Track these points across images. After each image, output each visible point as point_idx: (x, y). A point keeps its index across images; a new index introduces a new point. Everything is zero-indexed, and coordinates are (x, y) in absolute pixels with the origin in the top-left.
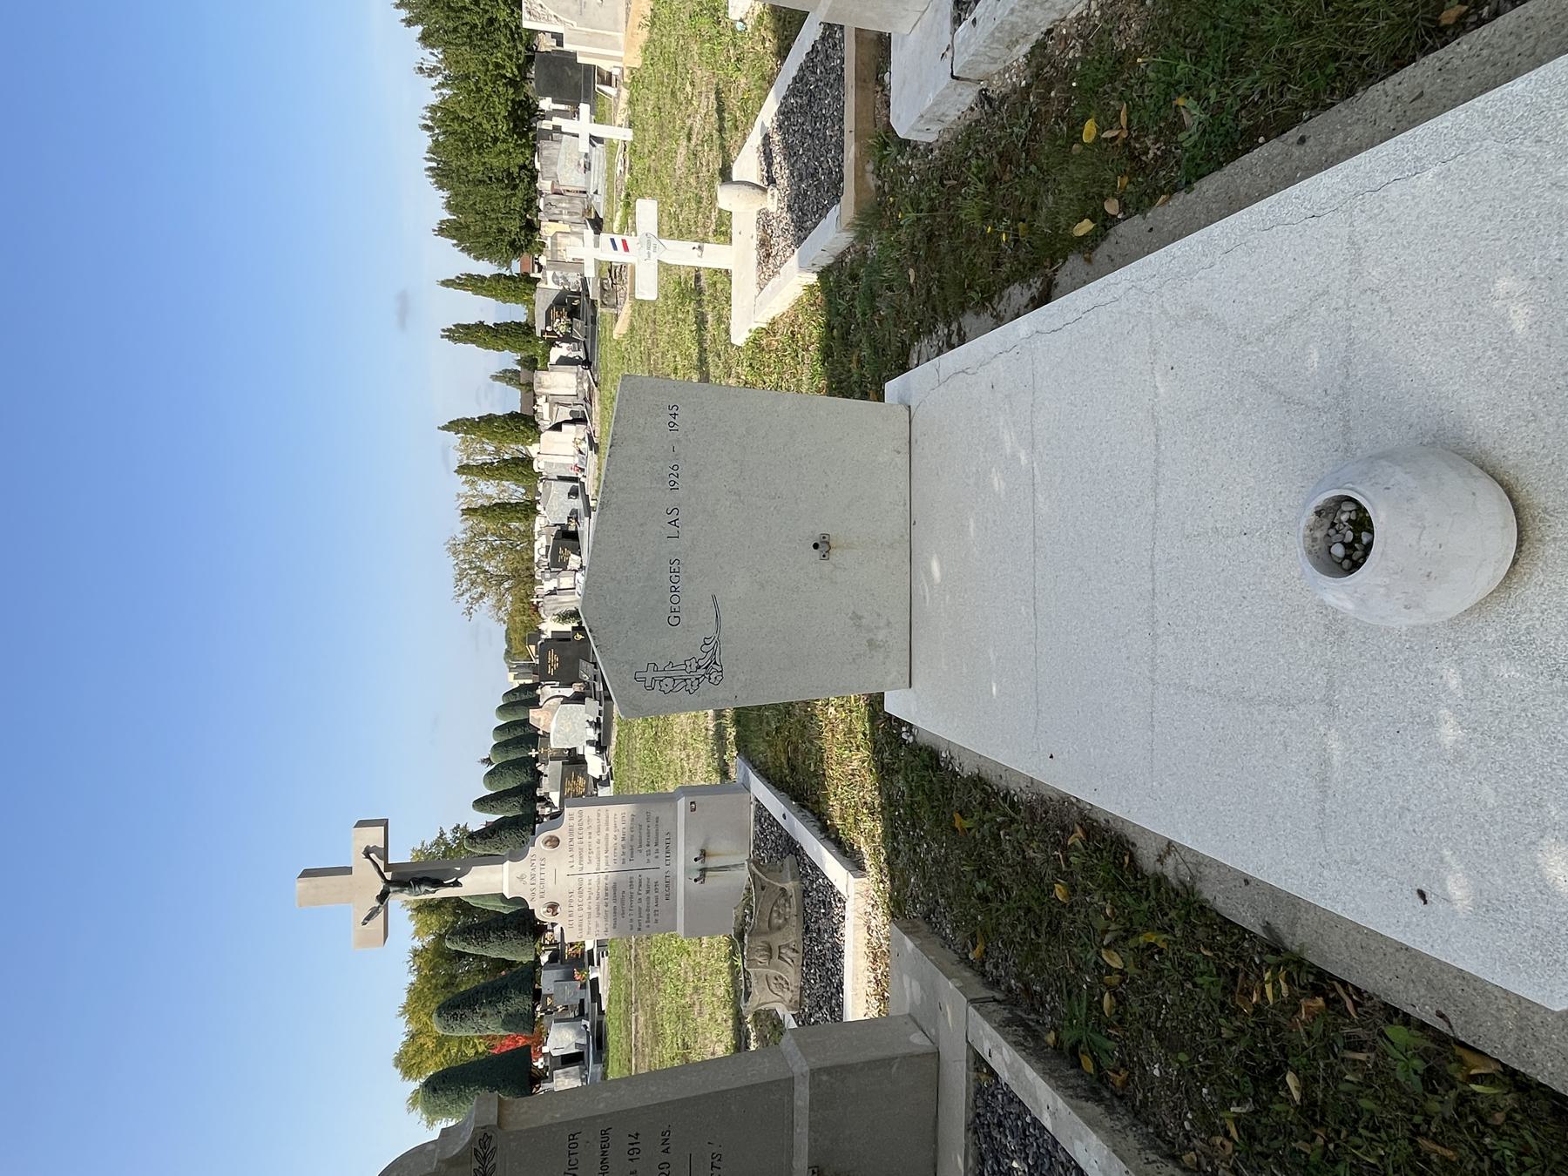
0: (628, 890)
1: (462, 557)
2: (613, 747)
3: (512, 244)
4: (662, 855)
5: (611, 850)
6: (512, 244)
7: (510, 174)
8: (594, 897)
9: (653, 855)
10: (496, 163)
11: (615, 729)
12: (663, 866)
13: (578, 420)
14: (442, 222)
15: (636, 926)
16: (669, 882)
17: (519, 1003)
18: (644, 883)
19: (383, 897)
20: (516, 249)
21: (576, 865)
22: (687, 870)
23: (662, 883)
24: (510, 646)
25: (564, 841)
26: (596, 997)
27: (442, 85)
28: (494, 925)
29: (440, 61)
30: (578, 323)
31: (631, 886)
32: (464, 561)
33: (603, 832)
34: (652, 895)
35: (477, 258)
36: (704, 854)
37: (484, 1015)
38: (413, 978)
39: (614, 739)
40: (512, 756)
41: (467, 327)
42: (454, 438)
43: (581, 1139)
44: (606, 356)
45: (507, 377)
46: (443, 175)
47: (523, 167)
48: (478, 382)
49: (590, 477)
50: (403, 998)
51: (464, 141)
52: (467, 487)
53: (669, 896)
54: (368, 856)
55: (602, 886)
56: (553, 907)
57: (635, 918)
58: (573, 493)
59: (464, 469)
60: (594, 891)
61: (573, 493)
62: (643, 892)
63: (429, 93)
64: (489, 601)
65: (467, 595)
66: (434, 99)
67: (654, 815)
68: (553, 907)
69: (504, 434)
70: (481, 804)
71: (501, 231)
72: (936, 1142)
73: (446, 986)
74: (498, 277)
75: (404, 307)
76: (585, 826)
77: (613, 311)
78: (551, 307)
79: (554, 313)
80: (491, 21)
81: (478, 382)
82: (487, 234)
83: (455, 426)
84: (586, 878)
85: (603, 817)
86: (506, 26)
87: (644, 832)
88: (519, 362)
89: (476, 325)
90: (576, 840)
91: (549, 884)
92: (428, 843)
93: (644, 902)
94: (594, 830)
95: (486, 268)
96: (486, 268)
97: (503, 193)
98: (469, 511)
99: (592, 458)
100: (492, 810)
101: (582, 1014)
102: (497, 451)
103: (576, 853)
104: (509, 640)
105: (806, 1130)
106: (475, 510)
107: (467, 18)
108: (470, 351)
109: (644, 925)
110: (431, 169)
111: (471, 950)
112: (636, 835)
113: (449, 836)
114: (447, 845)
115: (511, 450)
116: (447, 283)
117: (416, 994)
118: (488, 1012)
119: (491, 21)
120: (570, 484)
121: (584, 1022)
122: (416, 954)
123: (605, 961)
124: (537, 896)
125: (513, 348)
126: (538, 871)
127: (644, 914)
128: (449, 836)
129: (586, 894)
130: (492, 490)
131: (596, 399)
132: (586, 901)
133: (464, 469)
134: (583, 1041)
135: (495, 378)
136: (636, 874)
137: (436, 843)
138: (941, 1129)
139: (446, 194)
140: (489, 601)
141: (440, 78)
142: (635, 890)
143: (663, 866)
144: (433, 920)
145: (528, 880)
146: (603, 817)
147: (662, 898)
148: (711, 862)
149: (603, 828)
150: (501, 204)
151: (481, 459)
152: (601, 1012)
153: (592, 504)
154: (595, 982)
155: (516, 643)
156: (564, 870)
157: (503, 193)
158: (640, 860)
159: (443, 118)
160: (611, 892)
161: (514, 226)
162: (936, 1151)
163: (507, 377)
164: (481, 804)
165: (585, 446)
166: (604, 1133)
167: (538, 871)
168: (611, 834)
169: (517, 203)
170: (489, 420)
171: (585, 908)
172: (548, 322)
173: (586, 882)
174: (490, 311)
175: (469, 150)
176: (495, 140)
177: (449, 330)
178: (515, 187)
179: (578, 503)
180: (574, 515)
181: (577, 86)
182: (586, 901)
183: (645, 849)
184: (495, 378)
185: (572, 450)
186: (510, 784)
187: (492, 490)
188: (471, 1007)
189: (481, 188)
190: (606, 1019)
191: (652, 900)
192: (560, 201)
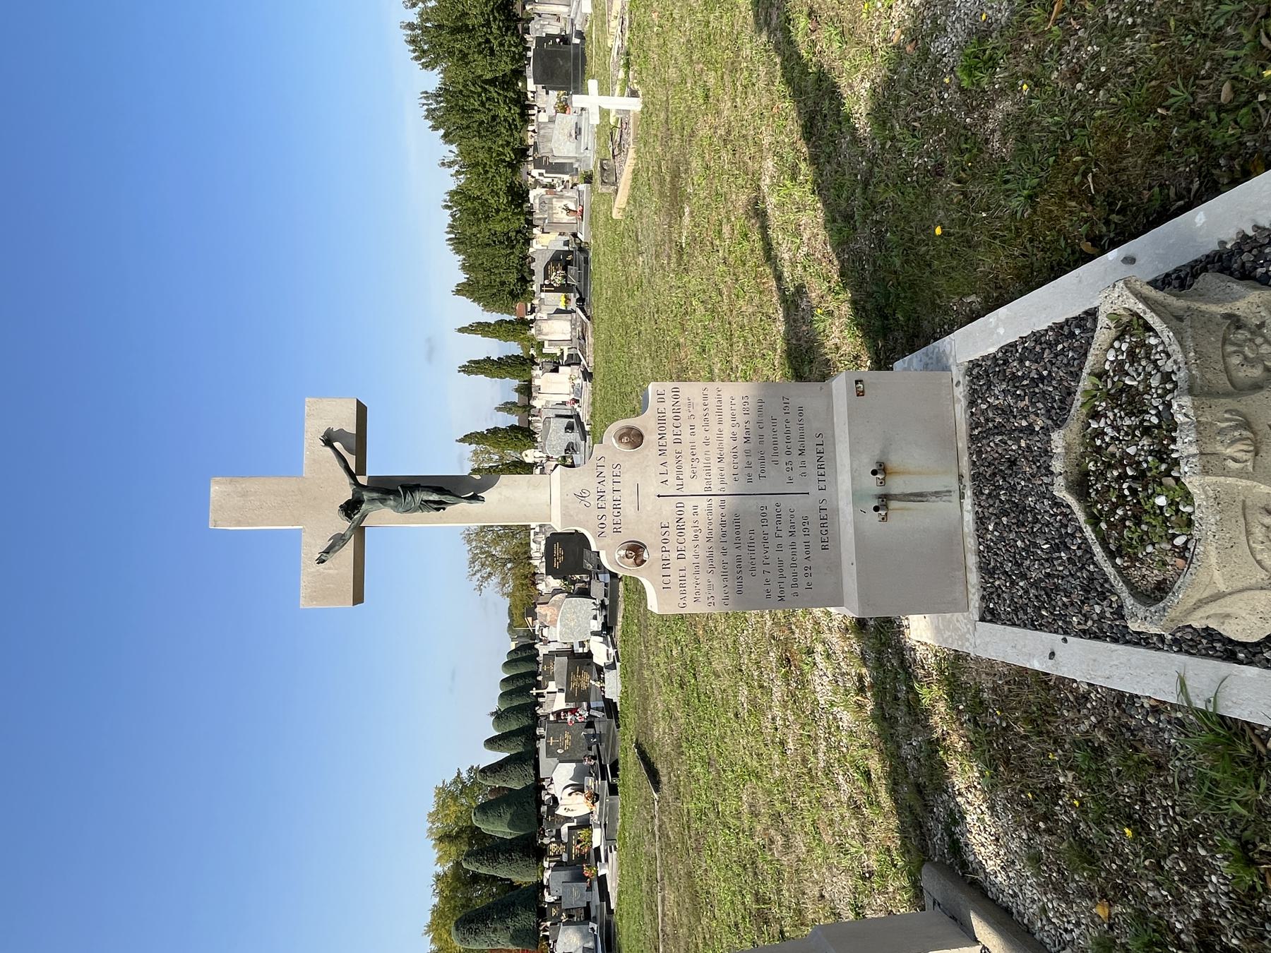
0: (759, 529)
1: (474, 544)
2: (619, 627)
3: (511, 293)
4: (812, 470)
5: (728, 459)
6: (511, 293)
7: (509, 238)
8: (702, 537)
9: (795, 474)
11: (621, 606)
12: (813, 490)
13: (573, 361)
15: (775, 593)
16: (826, 517)
17: (525, 919)
18: (785, 517)
19: (350, 508)
20: (514, 296)
21: (672, 478)
22: (857, 496)
23: (814, 519)
24: (512, 620)
25: (651, 437)
26: (604, 895)
27: (481, 328)
28: (503, 848)
29: (457, 156)
30: (572, 270)
31: (764, 521)
32: (476, 547)
33: (714, 428)
34: (800, 540)
36: (881, 469)
37: (495, 930)
38: (436, 900)
39: (620, 619)
40: (515, 703)
44: (598, 307)
45: (508, 407)
46: (459, 243)
47: (518, 232)
49: (585, 405)
50: (428, 918)
53: (828, 541)
55: (716, 518)
56: (636, 550)
57: (774, 576)
58: (570, 428)
60: (703, 525)
61: (570, 428)
62: (785, 534)
63: (449, 181)
64: (495, 580)
65: (478, 575)
66: (452, 185)
67: (795, 402)
68: (636, 550)
69: (506, 443)
70: (491, 743)
71: (503, 283)
73: (463, 906)
74: (500, 323)
76: (684, 414)
78: (548, 264)
79: (551, 267)
80: (494, 118)
83: (468, 438)
84: (689, 503)
85: (712, 401)
86: (505, 120)
87: (781, 427)
88: (516, 390)
89: (484, 360)
90: (670, 438)
91: (628, 509)
92: (448, 781)
93: (787, 551)
94: (698, 423)
96: (492, 317)
97: (503, 252)
99: (587, 386)
100: (499, 748)
101: (588, 917)
102: (501, 458)
103: (671, 461)
104: (511, 615)
107: (477, 117)
108: (481, 381)
109: (788, 591)
110: (450, 239)
111: (483, 870)
112: (767, 433)
113: (465, 775)
114: (463, 783)
115: (511, 455)
116: (462, 330)
117: (438, 913)
118: (499, 926)
119: (494, 118)
120: (567, 420)
121: (591, 924)
122: (439, 878)
123: (613, 856)
124: (609, 530)
125: (513, 376)
126: (608, 486)
127: (788, 573)
128: (465, 775)
129: (689, 533)
132: (689, 544)
134: (591, 945)
135: (499, 409)
136: (770, 502)
137: (455, 782)
139: (462, 257)
140: (495, 580)
141: (457, 167)
142: (771, 529)
143: (813, 490)
145: (592, 499)
146: (712, 401)
147: (816, 545)
148: (897, 485)
149: (713, 418)
152: (610, 911)
153: (587, 428)
154: (602, 880)
155: (517, 619)
156: (652, 487)
157: (503, 252)
158: (775, 480)
159: (459, 197)
160: (730, 530)
161: (513, 277)
163: (508, 407)
164: (491, 743)
167: (608, 486)
168: (727, 430)
169: (514, 260)
170: (495, 431)
171: (689, 554)
172: (546, 276)
173: (688, 510)
174: (494, 348)
175: (479, 220)
176: (498, 211)
178: (513, 247)
179: (575, 436)
181: (567, 74)
182: (689, 544)
183: (783, 459)
184: (499, 409)
185: (567, 388)
186: (514, 726)
188: (484, 922)
190: (616, 918)
191: (800, 548)
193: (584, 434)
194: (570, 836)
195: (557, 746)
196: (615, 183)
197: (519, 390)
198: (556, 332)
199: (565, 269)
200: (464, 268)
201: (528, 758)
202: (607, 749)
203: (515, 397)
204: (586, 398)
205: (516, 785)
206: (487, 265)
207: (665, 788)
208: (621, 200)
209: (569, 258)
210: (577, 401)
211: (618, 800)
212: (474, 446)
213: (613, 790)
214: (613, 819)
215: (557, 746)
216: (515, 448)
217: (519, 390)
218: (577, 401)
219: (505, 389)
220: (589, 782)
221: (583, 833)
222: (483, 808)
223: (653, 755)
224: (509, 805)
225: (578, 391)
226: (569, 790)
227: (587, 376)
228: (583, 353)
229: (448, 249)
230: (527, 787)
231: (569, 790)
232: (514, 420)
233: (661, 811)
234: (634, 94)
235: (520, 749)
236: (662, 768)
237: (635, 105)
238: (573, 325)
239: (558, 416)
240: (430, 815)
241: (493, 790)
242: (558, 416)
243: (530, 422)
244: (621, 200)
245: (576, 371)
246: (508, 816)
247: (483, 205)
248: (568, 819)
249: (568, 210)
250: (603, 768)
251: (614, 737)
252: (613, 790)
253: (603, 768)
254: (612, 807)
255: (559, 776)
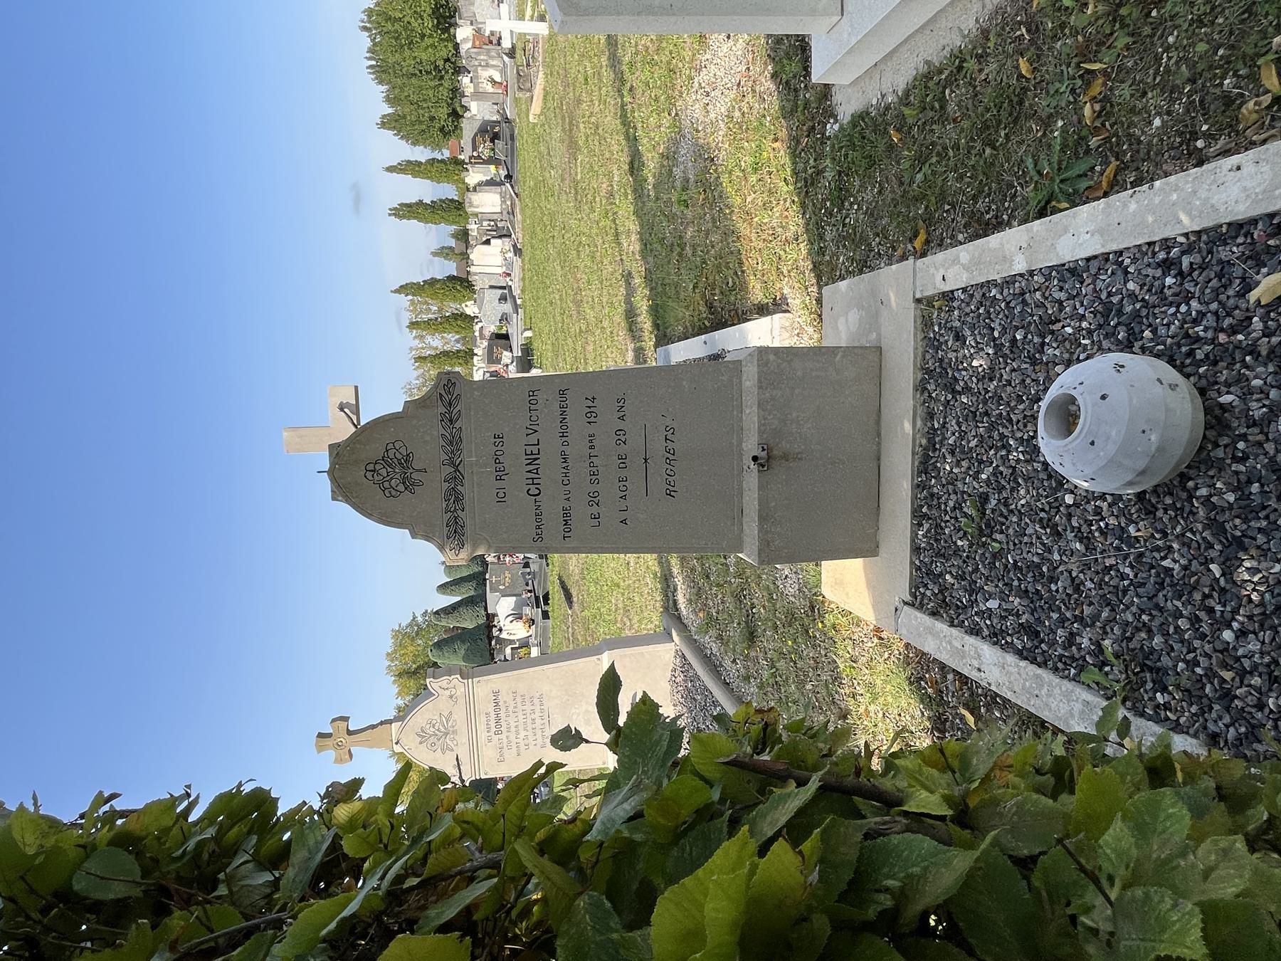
3: (442, 129)
6: (442, 129)
7: (436, 67)
10: (424, 57)
14: (384, 117)
20: (445, 133)
30: (500, 144)
35: (414, 144)
41: (409, 206)
42: (404, 300)
43: (540, 396)
44: (527, 182)
46: (382, 71)
47: (447, 60)
48: (417, 251)
51: (397, 39)
52: (417, 341)
54: (342, 410)
58: (503, 299)
59: (413, 325)
61: (503, 299)
69: (444, 294)
70: (443, 588)
71: (432, 119)
72: (879, 435)
74: (432, 161)
75: (358, 197)
77: (528, 94)
78: (476, 135)
79: (479, 139)
81: (417, 251)
82: (421, 123)
83: (404, 289)
88: (453, 236)
89: (417, 204)
92: (404, 624)
95: (421, 154)
96: (421, 154)
97: (432, 84)
98: (420, 359)
99: (517, 262)
102: (440, 310)
105: (755, 408)
106: (425, 358)
110: (371, 67)
113: (420, 619)
114: (418, 626)
115: (451, 307)
116: (390, 169)
128: (420, 619)
130: (436, 342)
131: (517, 210)
133: (413, 325)
135: (435, 254)
137: (410, 625)
138: (883, 424)
139: (385, 88)
144: (412, 683)
150: (431, 93)
151: (425, 317)
153: (519, 302)
157: (432, 84)
161: (443, 112)
162: (879, 444)
164: (443, 588)
165: (510, 255)
166: (562, 393)
169: (445, 93)
170: (432, 282)
172: (475, 148)
175: (402, 46)
176: (423, 36)
177: (395, 209)
178: (442, 78)
179: (507, 307)
180: (504, 318)
184: (435, 254)
185: (499, 260)
187: (436, 342)
189: (413, 80)
192: (478, 54)
193: (516, 308)
194: (513, 655)
195: (498, 583)
196: (530, 90)
197: (455, 236)
198: (488, 203)
199: (492, 141)
200: (388, 100)
201: (477, 600)
202: (539, 584)
203: (452, 243)
204: (516, 273)
205: (470, 625)
206: (414, 98)
207: (576, 606)
208: (536, 108)
209: (497, 129)
210: (509, 275)
211: (550, 622)
212: (410, 297)
213: (546, 615)
214: (546, 639)
215: (498, 583)
216: (455, 299)
217: (455, 236)
218: (509, 275)
219: (442, 234)
220: (527, 611)
221: (522, 651)
222: (439, 645)
223: (569, 584)
224: (463, 642)
225: (509, 265)
226: (511, 618)
227: (517, 251)
228: (514, 228)
229: (368, 80)
230: (478, 627)
231: (511, 618)
232: (451, 268)
233: (573, 622)
234: (542, 18)
235: (472, 593)
236: (574, 592)
237: (542, 29)
238: (503, 197)
239: (492, 287)
240: (388, 654)
241: (447, 630)
242: (492, 287)
243: (468, 272)
244: (536, 108)
245: (506, 244)
246: (463, 652)
247: (405, 29)
248: (512, 642)
249: (493, 82)
250: (537, 598)
251: (546, 573)
252: (546, 615)
253: (537, 598)
254: (545, 629)
255: (503, 607)
